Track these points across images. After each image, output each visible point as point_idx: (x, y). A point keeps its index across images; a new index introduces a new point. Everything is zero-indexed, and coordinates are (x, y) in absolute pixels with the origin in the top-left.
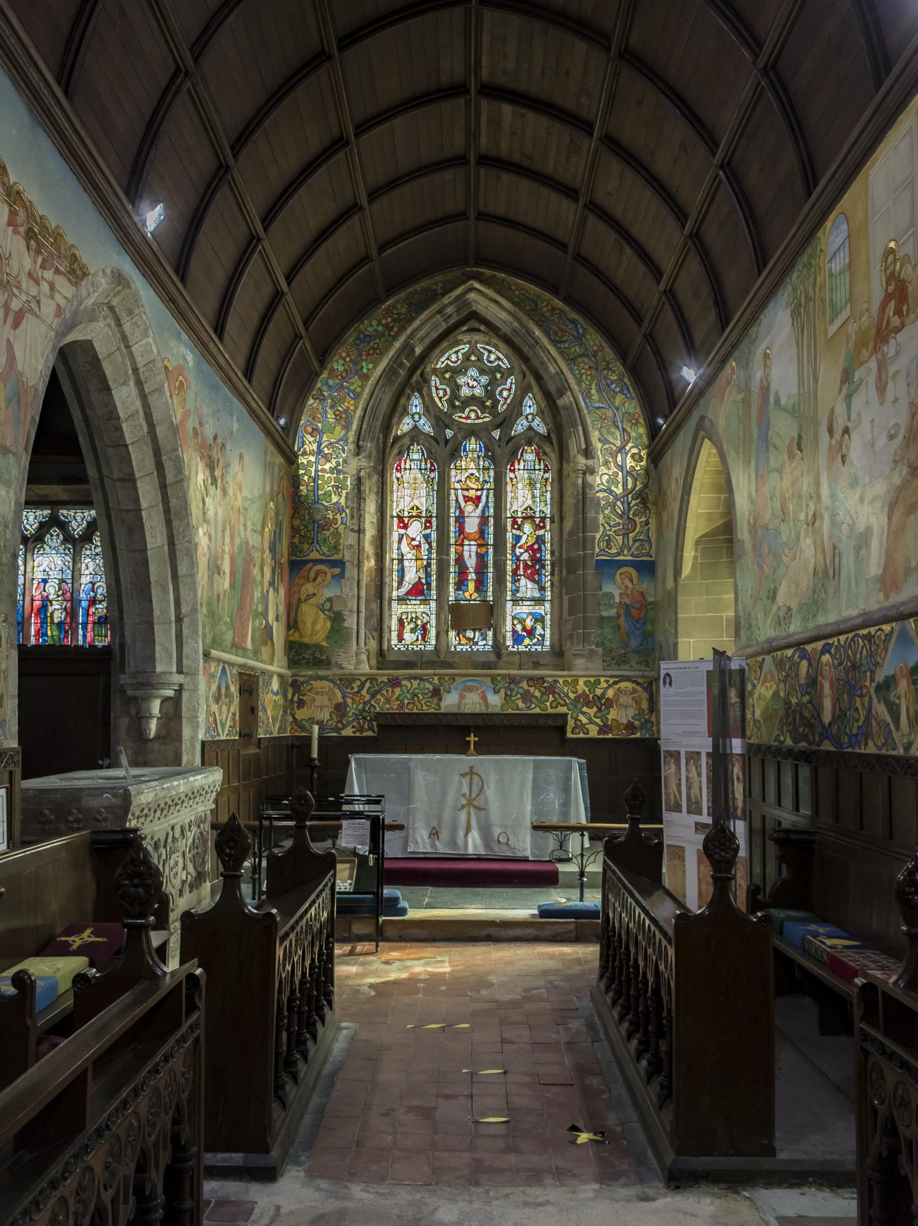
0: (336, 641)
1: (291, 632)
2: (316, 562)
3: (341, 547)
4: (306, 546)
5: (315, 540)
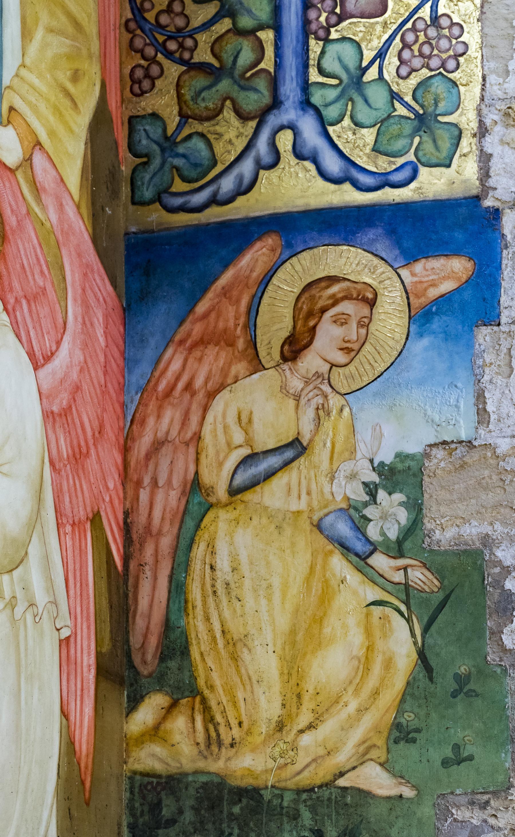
0: (458, 758)
1: (145, 715)
2: (299, 228)
3: (467, 118)
4: (231, 134)
5: (290, 89)
